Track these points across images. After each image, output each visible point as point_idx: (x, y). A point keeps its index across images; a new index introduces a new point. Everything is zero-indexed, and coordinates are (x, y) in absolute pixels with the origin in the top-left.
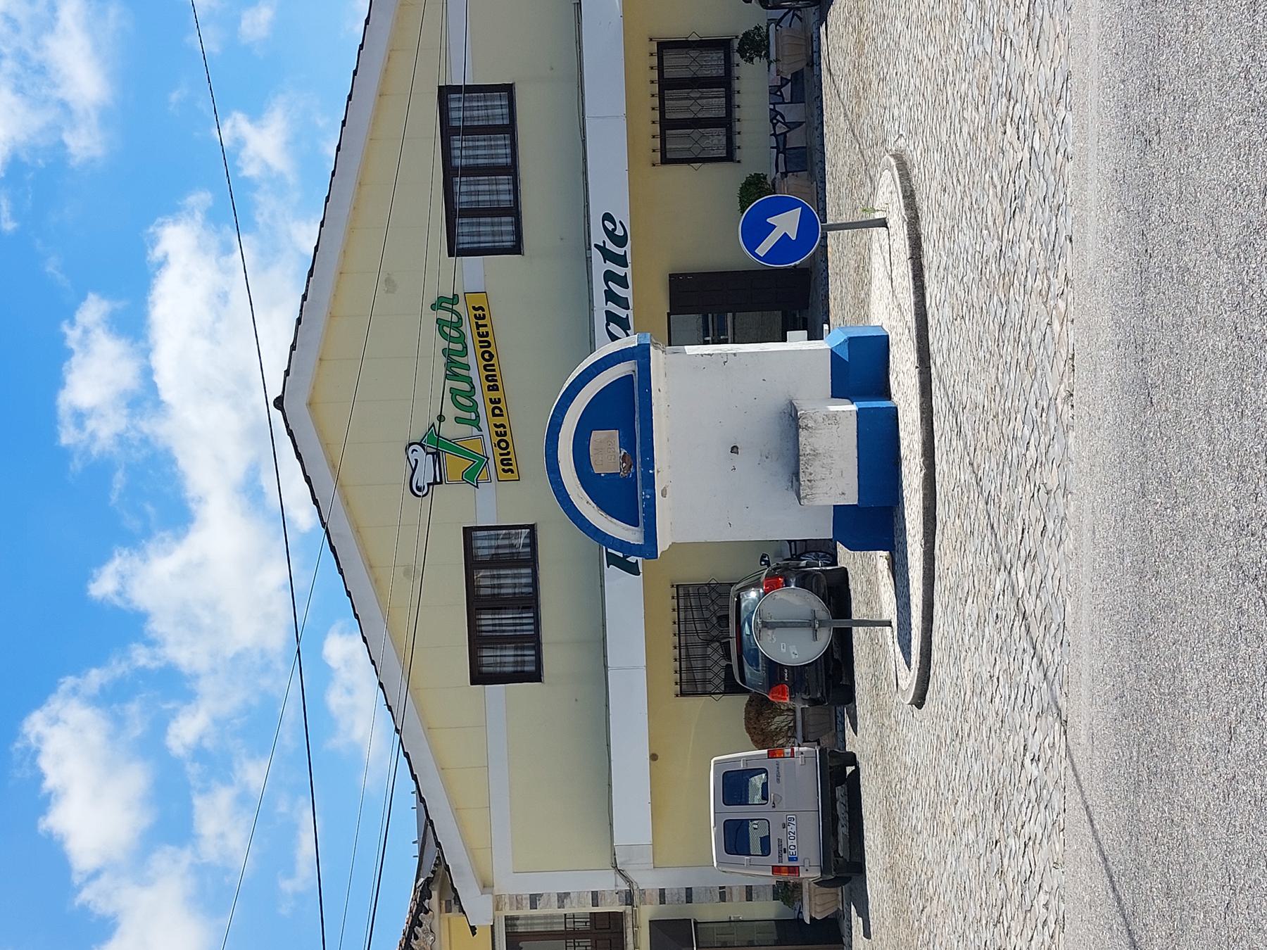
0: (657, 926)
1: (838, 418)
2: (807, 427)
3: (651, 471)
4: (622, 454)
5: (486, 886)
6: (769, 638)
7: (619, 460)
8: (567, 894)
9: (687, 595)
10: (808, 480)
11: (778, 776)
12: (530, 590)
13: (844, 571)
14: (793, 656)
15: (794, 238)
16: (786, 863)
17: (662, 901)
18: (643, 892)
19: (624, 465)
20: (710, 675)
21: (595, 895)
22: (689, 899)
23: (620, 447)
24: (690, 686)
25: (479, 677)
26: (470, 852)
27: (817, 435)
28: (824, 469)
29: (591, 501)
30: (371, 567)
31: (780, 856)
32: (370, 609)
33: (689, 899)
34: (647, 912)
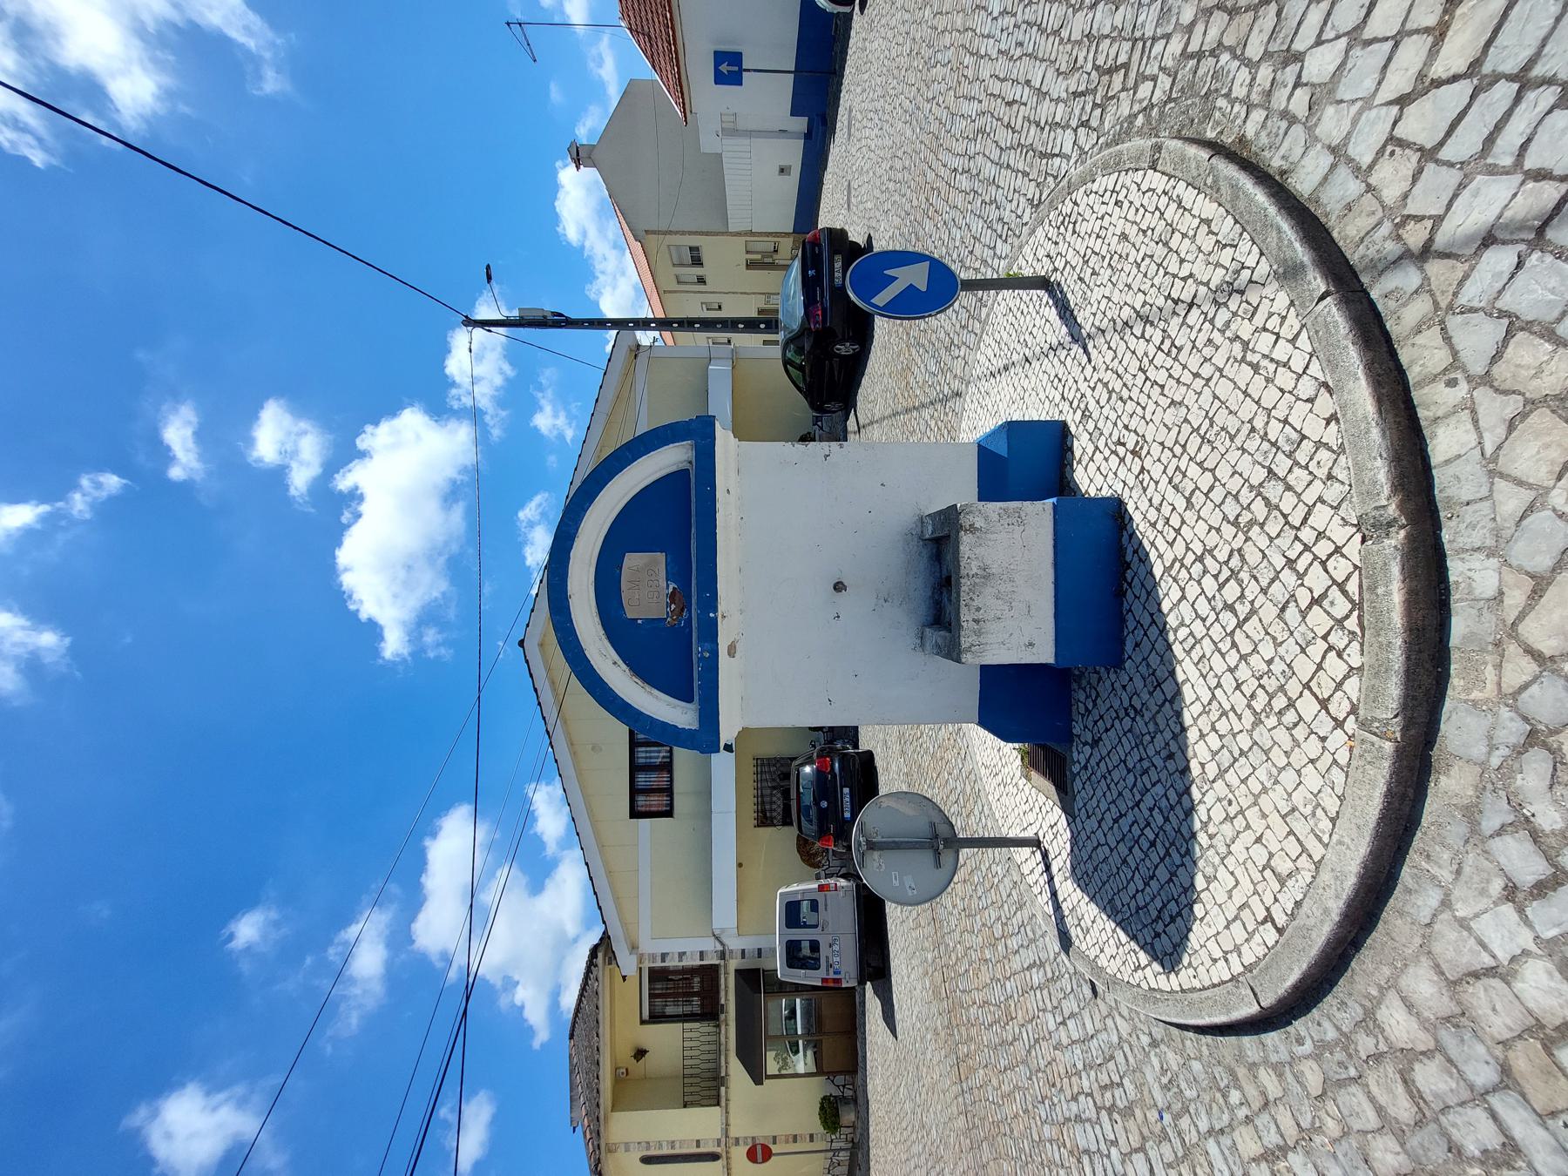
0: (739, 973)
1: (1023, 514)
2: (972, 529)
3: (712, 615)
4: (670, 590)
5: (634, 948)
6: (876, 865)
7: (665, 600)
8: (684, 953)
9: (762, 765)
10: (974, 620)
11: (826, 905)
12: (668, 760)
13: (869, 755)
14: (910, 893)
15: (924, 289)
16: (832, 976)
17: (743, 957)
18: (731, 951)
19: (673, 606)
20: (774, 814)
21: (702, 953)
22: (760, 956)
23: (667, 580)
24: (764, 820)
25: (635, 814)
26: (624, 924)
27: (990, 543)
28: (1000, 602)
29: (620, 662)
30: (572, 744)
31: (828, 971)
32: (569, 771)
33: (760, 956)
34: (734, 964)
